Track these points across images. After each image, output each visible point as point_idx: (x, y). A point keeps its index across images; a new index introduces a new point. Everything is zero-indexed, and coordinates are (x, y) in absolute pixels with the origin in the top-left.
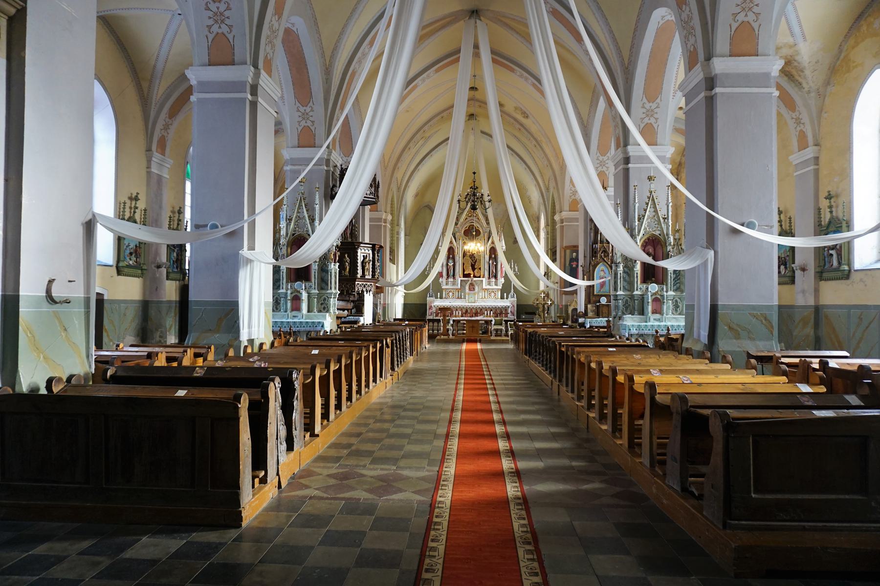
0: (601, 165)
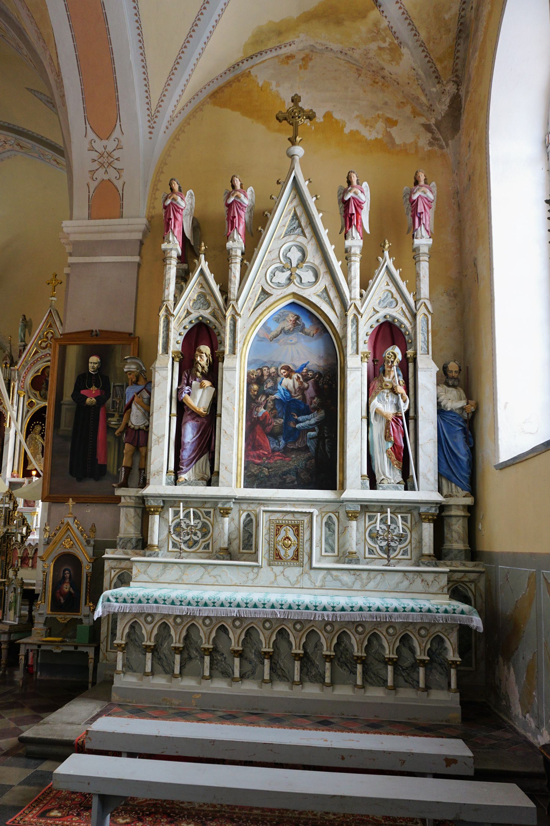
0: (102, 165)
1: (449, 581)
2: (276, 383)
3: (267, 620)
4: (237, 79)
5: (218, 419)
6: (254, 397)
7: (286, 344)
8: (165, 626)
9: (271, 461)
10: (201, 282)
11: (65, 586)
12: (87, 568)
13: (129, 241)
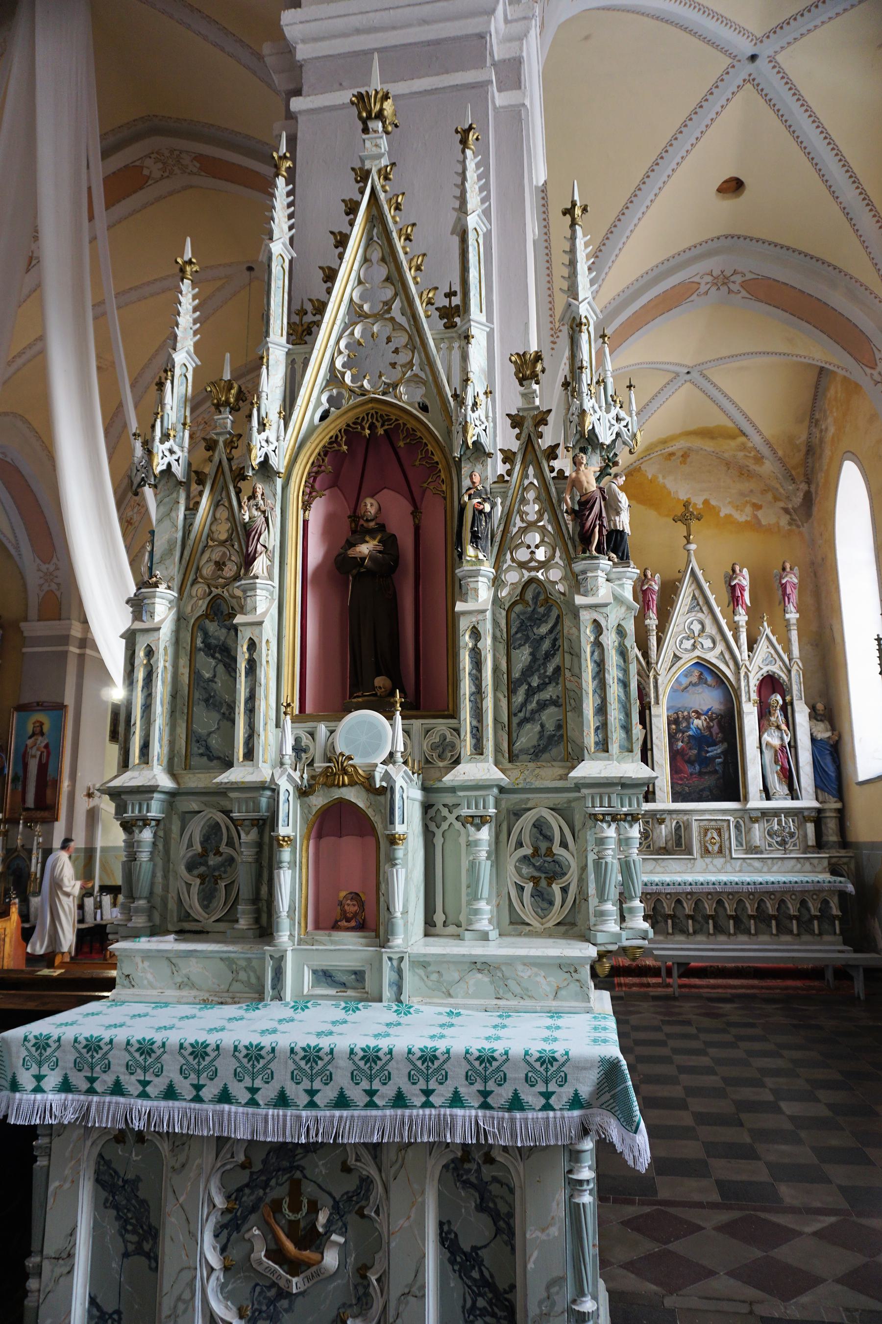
0: (46, 580)
1: (829, 864)
2: (689, 723)
3: (709, 893)
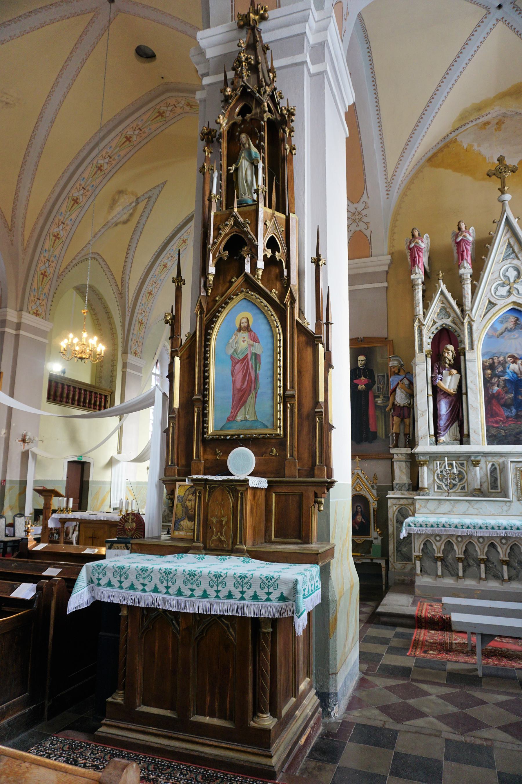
2: (505, 368)
4: (447, 146)
5: (464, 397)
6: (489, 379)
7: (510, 339)
8: (449, 543)
9: (507, 425)
10: (442, 299)
11: (358, 517)
12: (373, 505)
13: (378, 273)
